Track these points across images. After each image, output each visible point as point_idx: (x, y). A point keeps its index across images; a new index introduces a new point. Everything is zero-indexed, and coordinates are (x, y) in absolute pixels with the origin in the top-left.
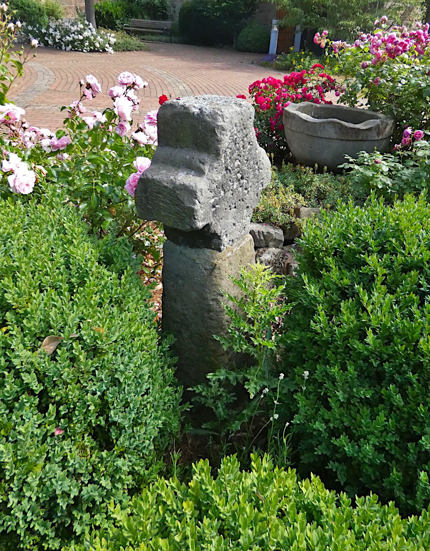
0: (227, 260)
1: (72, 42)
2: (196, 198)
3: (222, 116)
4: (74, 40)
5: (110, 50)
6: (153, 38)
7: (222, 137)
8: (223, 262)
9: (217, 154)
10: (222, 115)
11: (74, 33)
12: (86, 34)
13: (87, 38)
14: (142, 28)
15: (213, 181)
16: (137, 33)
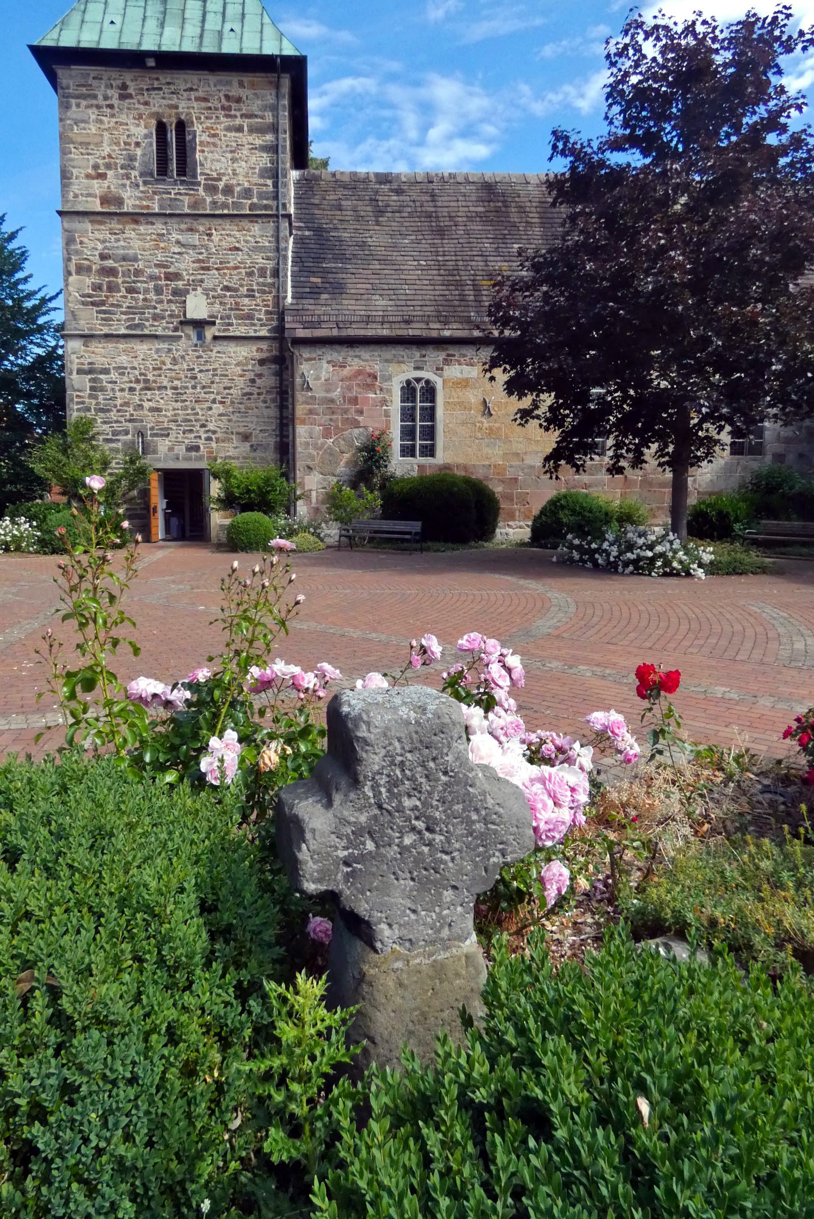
0: (393, 976)
1: (635, 562)
3: (368, 724)
4: (639, 559)
5: (700, 573)
6: (805, 550)
7: (364, 755)
8: (383, 976)
9: (355, 782)
11: (641, 548)
12: (659, 549)
13: (662, 555)
14: (777, 535)
15: (344, 821)
16: (756, 543)
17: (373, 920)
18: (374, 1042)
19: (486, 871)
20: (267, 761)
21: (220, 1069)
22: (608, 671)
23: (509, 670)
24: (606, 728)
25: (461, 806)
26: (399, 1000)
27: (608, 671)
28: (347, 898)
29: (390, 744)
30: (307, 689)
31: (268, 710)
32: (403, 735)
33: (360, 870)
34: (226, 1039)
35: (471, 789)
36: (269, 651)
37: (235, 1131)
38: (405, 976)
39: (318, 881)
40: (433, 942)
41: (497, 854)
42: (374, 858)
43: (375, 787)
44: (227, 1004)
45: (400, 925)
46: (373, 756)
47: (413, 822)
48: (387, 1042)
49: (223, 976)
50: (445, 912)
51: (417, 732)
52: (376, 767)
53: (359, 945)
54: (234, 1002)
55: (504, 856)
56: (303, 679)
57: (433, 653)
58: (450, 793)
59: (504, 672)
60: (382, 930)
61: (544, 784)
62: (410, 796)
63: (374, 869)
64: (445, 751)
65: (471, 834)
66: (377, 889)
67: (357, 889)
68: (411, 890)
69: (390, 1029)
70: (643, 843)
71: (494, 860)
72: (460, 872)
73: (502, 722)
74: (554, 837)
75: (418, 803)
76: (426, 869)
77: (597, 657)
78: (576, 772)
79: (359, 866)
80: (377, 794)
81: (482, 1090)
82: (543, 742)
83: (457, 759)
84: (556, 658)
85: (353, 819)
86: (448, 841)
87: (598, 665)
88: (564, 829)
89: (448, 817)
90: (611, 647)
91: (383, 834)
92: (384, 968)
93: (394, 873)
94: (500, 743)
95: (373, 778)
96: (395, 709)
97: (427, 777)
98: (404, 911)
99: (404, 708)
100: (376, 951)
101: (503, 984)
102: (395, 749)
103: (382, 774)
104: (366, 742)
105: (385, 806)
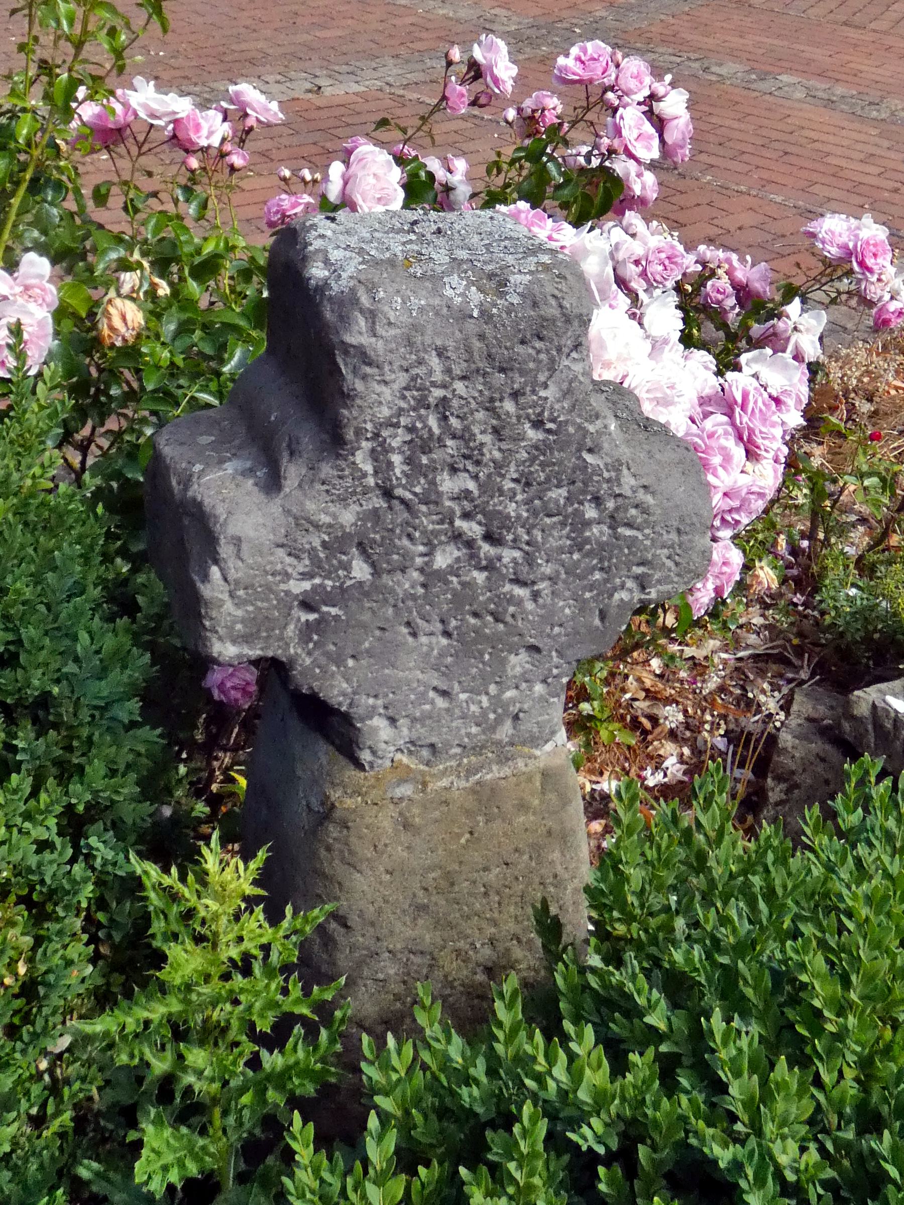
0: (392, 811)
2: (216, 562)
3: (372, 316)
7: (359, 386)
10: (371, 312)
17: (356, 712)
18: (346, 926)
19: (603, 616)
20: (117, 322)
21: (31, 960)
22: (840, 90)
23: (660, 123)
24: (849, 253)
25: (564, 492)
26: (400, 852)
27: (840, 90)
28: (306, 671)
29: (420, 362)
30: (205, 150)
31: (115, 190)
32: (451, 344)
33: (337, 618)
34: (41, 905)
35: (589, 458)
36: (121, 69)
37: (60, 1056)
38: (416, 811)
39: (246, 639)
40: (477, 750)
41: (630, 584)
42: (367, 594)
43: (379, 455)
44: (43, 846)
45: (414, 720)
46: (379, 388)
47: (458, 523)
48: (373, 924)
49: (34, 793)
50: (509, 694)
51: (482, 337)
52: (385, 412)
53: (324, 752)
54: (58, 841)
55: (643, 588)
56: (198, 127)
57: (496, 81)
58: (543, 465)
59: (649, 128)
60: (376, 730)
61: (730, 415)
62: (454, 470)
63: (366, 617)
64: (542, 378)
65: (579, 546)
66: (369, 653)
67: (327, 655)
68: (441, 655)
69: (380, 902)
70: (883, 480)
71: (624, 595)
72: (549, 618)
73: (637, 249)
74: (737, 522)
75: (471, 485)
76: (476, 615)
77: (819, 55)
78: (786, 366)
79: (334, 611)
80: (383, 467)
81: (594, 1121)
82: (708, 273)
83: (567, 393)
84: (733, 54)
85: (325, 519)
86: (529, 560)
87: (821, 75)
88: (759, 505)
89: (535, 513)
90: (852, 33)
91: (393, 548)
92: (374, 794)
93: (408, 624)
94: (634, 298)
95: (377, 435)
96: (435, 280)
97: (496, 431)
98: (424, 694)
99: (454, 279)
100: (360, 766)
101: (636, 875)
102: (430, 372)
103: (397, 425)
104: (365, 357)
105: (399, 492)
